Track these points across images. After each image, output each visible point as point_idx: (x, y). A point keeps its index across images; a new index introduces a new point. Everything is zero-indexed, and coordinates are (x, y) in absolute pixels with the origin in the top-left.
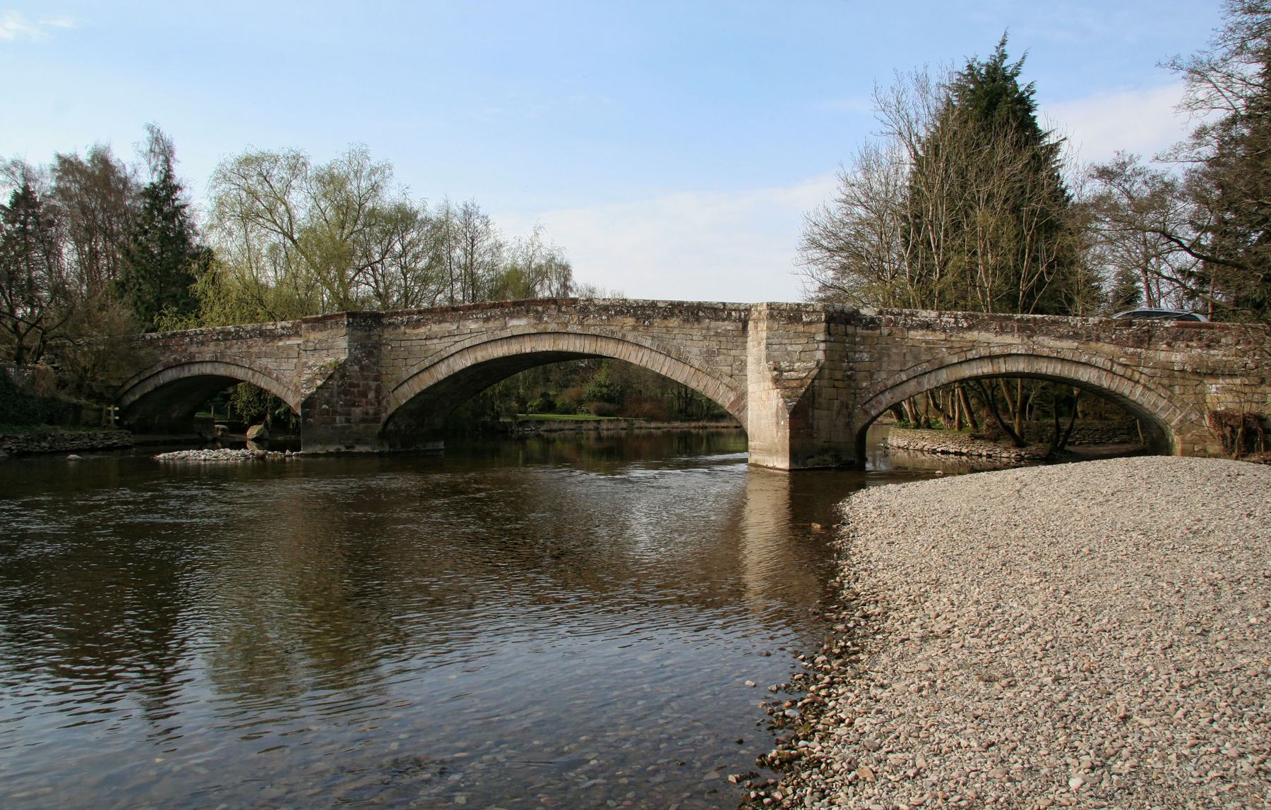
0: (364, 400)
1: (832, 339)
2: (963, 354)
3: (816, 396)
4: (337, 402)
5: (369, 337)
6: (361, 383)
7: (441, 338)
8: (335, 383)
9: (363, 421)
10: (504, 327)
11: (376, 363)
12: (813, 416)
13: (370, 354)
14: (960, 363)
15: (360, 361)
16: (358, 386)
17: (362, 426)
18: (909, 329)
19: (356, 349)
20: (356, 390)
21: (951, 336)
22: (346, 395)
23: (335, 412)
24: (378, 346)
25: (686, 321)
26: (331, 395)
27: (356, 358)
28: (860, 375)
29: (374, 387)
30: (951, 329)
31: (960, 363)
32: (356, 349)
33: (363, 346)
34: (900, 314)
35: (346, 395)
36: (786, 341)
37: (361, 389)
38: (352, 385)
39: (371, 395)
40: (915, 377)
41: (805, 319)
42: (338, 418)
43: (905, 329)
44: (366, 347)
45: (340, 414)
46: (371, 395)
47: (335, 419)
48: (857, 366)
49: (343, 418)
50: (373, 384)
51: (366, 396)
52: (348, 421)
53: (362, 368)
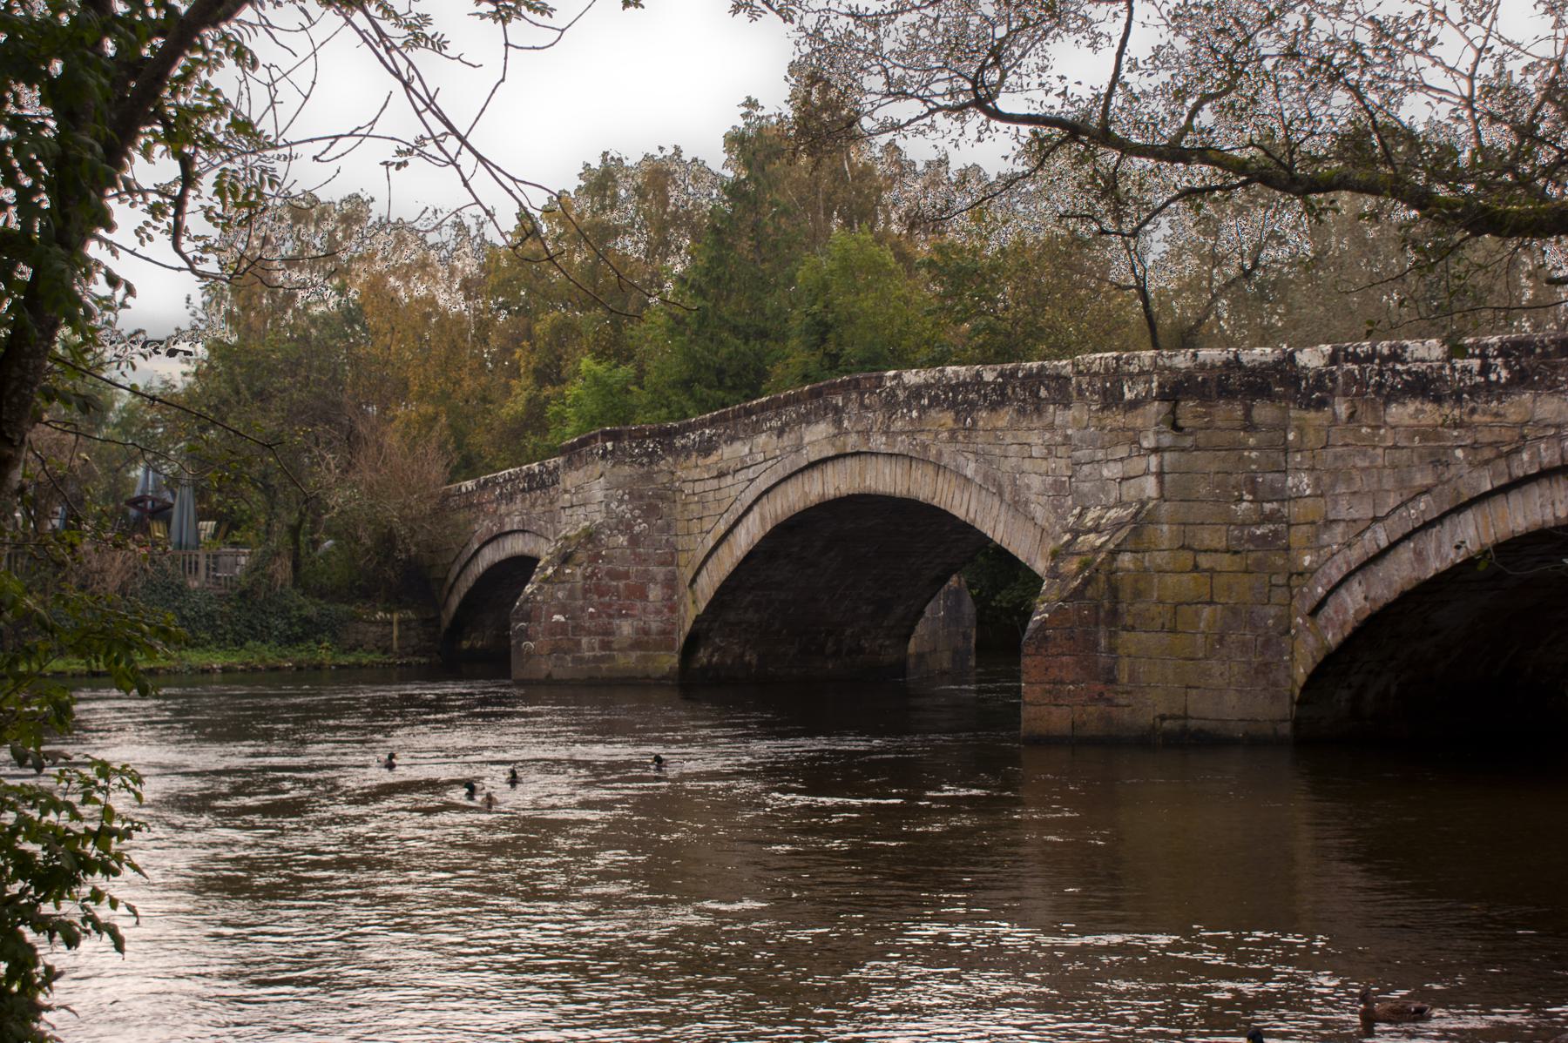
0: (639, 605)
1: (1188, 441)
2: (1502, 464)
3: (1126, 594)
4: (583, 609)
5: (648, 477)
6: (633, 569)
7: (736, 471)
8: (579, 571)
9: (636, 645)
10: (798, 448)
11: (668, 528)
12: (1112, 649)
13: (650, 511)
14: (1503, 490)
15: (630, 527)
16: (626, 575)
17: (635, 655)
18: (1388, 400)
19: (621, 501)
20: (621, 584)
21: (1473, 411)
22: (601, 595)
23: (578, 629)
24: (667, 494)
25: (1021, 412)
26: (571, 595)
27: (621, 520)
28: (1298, 535)
29: (660, 577)
30: (1474, 391)
31: (1503, 490)
32: (621, 501)
33: (636, 496)
34: (1369, 358)
35: (601, 595)
36: (1100, 455)
37: (632, 582)
38: (613, 575)
39: (655, 593)
40: (1407, 537)
41: (1128, 396)
42: (584, 640)
43: (1380, 400)
44: (641, 497)
45: (589, 633)
46: (655, 593)
47: (578, 643)
48: (1293, 510)
49: (596, 640)
50: (659, 572)
51: (644, 597)
52: (605, 645)
53: (634, 541)
